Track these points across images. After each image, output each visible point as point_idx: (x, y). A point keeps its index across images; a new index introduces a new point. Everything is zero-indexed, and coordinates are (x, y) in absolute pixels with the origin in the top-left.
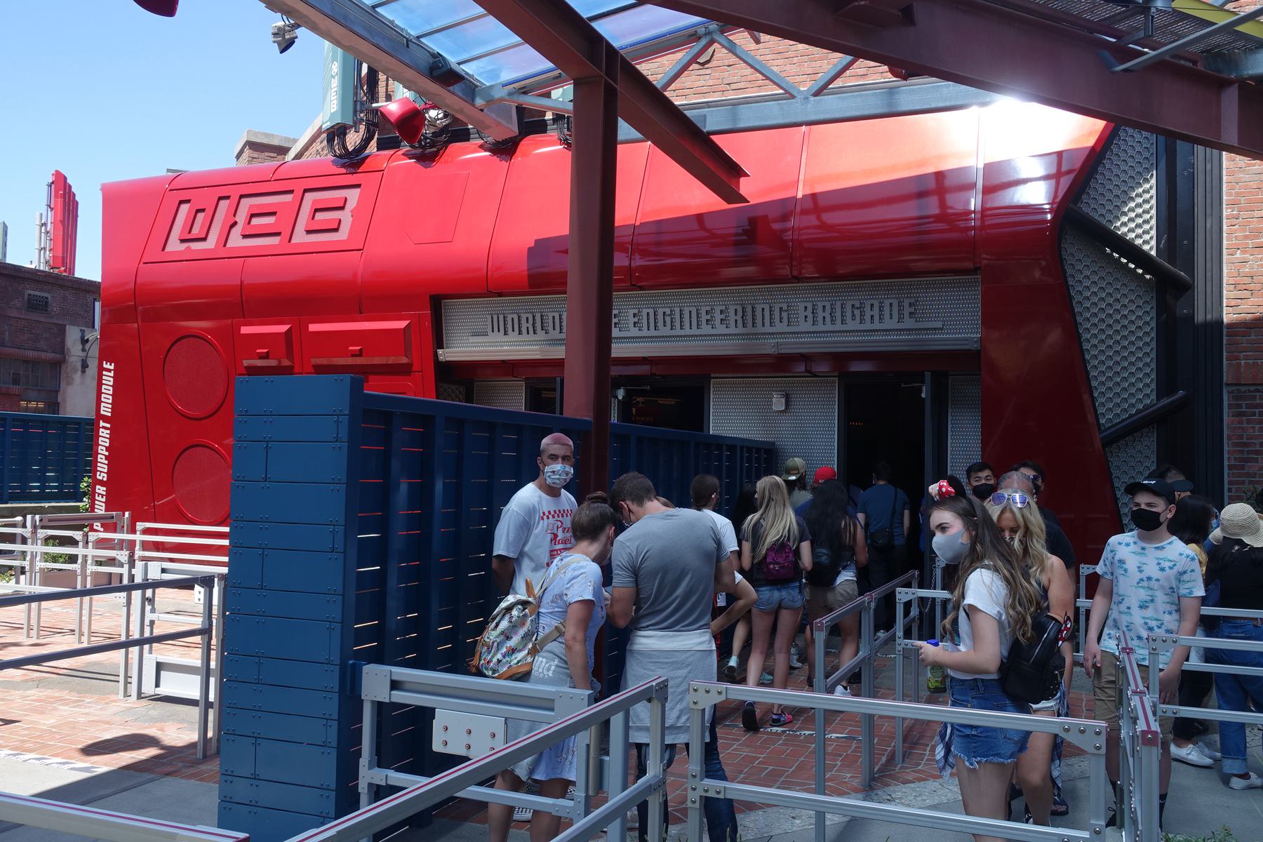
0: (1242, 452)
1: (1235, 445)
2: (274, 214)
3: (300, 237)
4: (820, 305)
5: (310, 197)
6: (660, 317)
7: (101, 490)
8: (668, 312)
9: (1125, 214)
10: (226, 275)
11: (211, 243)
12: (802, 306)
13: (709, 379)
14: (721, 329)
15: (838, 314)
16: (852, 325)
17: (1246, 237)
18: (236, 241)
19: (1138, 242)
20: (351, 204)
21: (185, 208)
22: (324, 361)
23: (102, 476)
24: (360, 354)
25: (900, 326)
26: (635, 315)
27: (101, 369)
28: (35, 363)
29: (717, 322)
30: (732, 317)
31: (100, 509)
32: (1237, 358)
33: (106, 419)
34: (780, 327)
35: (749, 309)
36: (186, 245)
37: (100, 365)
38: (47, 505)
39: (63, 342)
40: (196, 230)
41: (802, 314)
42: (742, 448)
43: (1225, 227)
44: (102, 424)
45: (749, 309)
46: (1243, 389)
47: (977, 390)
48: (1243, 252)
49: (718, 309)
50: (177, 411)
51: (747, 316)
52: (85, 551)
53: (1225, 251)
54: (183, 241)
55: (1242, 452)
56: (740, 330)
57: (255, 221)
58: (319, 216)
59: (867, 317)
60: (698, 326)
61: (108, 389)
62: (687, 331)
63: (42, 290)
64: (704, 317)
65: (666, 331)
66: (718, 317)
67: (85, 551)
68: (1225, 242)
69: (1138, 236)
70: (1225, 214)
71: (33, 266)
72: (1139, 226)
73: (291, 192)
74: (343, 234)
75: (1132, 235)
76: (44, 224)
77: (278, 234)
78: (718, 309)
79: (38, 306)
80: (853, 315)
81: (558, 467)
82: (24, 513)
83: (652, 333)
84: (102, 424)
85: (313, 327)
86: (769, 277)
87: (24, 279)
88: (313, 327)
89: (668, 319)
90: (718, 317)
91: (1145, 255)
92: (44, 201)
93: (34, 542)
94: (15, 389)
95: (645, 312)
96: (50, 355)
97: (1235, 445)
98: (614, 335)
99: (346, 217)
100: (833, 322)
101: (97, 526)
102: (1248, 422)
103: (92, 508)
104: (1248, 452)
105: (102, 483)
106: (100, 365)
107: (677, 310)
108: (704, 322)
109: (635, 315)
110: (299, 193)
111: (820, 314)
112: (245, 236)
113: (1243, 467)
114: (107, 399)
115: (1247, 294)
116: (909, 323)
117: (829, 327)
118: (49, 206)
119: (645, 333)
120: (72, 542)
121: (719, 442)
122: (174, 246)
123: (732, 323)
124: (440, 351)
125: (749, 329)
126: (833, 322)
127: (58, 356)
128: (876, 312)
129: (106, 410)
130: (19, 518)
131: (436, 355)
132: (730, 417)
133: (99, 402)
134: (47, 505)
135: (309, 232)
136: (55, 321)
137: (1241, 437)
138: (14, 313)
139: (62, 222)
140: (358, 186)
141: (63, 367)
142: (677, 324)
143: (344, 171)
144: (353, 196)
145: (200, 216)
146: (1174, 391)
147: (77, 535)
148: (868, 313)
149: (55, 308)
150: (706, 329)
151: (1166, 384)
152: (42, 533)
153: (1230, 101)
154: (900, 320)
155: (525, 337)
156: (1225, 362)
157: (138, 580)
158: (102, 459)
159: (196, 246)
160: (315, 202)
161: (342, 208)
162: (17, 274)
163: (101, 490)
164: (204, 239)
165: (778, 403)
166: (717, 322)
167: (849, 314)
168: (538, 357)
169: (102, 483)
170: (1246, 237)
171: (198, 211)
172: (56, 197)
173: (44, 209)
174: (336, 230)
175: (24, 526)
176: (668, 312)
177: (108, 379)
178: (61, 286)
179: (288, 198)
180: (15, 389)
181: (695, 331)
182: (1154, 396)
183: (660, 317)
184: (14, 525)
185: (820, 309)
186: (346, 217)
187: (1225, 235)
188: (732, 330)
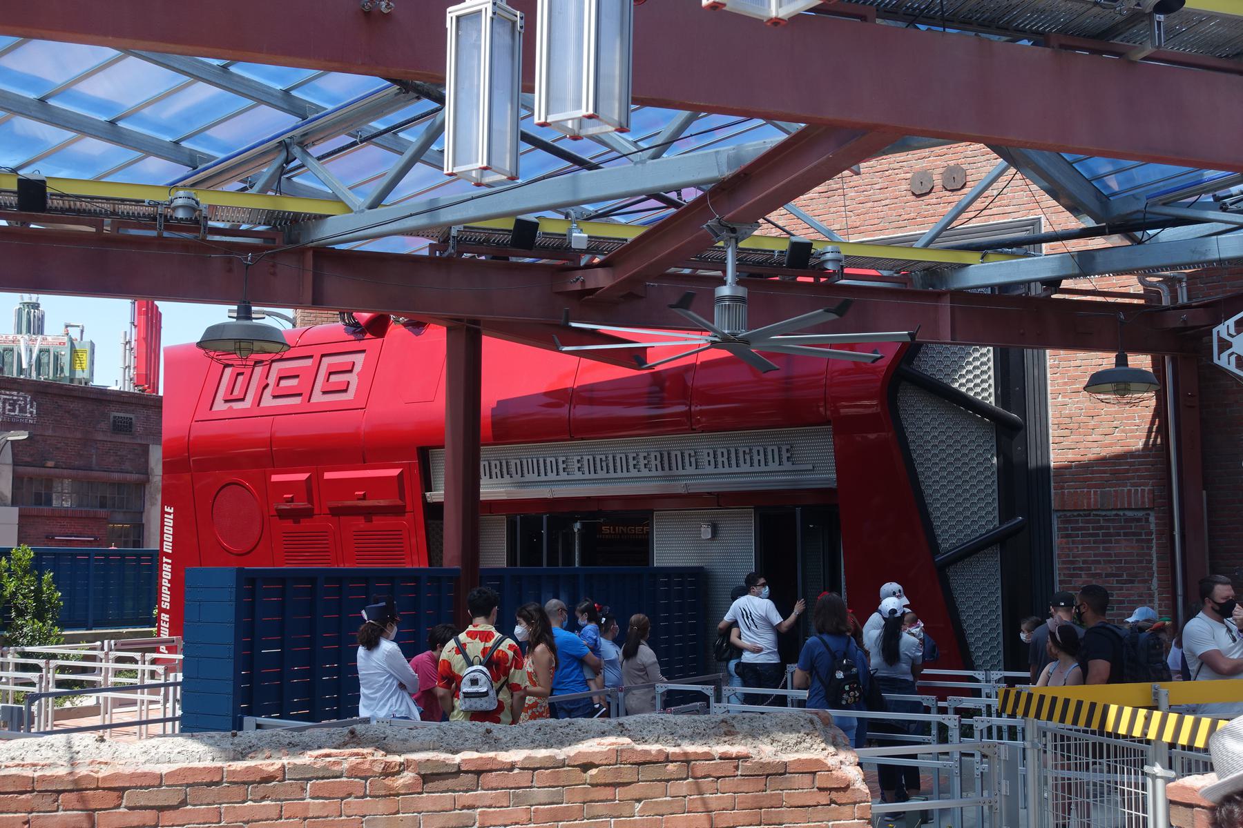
0: (1068, 569)
1: (1064, 562)
2: (297, 376)
3: (318, 397)
5: (326, 361)
7: (165, 617)
9: (969, 363)
10: (262, 429)
11: (247, 404)
12: (706, 452)
14: (645, 472)
16: (745, 468)
17: (1065, 384)
18: (268, 401)
19: (963, 390)
20: (357, 369)
21: (228, 371)
22: (339, 504)
23: (166, 606)
24: (364, 498)
25: (781, 468)
27: (163, 513)
28: (120, 485)
30: (653, 462)
31: (165, 635)
32: (1062, 488)
33: (168, 555)
34: (690, 470)
35: (666, 455)
36: (228, 405)
37: (163, 509)
38: (125, 631)
39: (147, 462)
40: (236, 392)
43: (1049, 375)
44: (165, 560)
45: (666, 455)
46: (1068, 514)
47: (863, 515)
48: (1064, 397)
50: (224, 548)
51: (665, 461)
52: (143, 667)
53: (1049, 396)
54: (226, 401)
55: (1068, 569)
56: (660, 473)
57: (284, 383)
58: (333, 378)
61: (169, 530)
62: (619, 474)
63: (126, 412)
67: (143, 667)
68: (1049, 388)
69: (971, 389)
70: (1049, 363)
71: (117, 388)
72: (976, 377)
73: (311, 357)
74: (350, 396)
76: (129, 342)
77: (300, 395)
78: (641, 455)
79: (123, 427)
82: (101, 637)
83: (593, 476)
84: (165, 560)
85: (328, 475)
86: (685, 424)
87: (110, 401)
88: (328, 475)
89: (604, 464)
90: (642, 462)
92: (128, 319)
93: (107, 661)
94: (102, 512)
95: (586, 458)
96: (134, 477)
97: (1064, 562)
99: (353, 379)
101: (163, 648)
102: (1074, 542)
103: (159, 634)
104: (1074, 569)
105: (165, 611)
106: (163, 509)
110: (317, 357)
111: (720, 459)
112: (275, 397)
113: (1070, 582)
114: (168, 538)
115: (1067, 432)
116: (787, 466)
117: (727, 470)
118: (133, 323)
119: (587, 476)
120: (132, 660)
122: (220, 406)
124: (428, 494)
125: (667, 472)
127: (142, 477)
128: (762, 457)
129: (168, 548)
130: (98, 643)
131: (424, 496)
133: (162, 541)
134: (125, 631)
135: (324, 393)
136: (139, 441)
137: (1068, 555)
138: (100, 437)
139: (145, 339)
140: (364, 351)
141: (147, 486)
143: (352, 337)
144: (359, 359)
145: (240, 378)
146: (1014, 516)
147: (137, 655)
149: (138, 428)
150: (634, 473)
151: (1006, 511)
152: (113, 654)
153: (946, 304)
155: (494, 480)
156: (1053, 491)
157: (171, 688)
158: (165, 590)
159: (237, 406)
160: (330, 365)
161: (351, 371)
162: (103, 397)
163: (165, 617)
164: (243, 400)
165: (706, 533)
169: (165, 611)
170: (1065, 384)
171: (238, 374)
172: (139, 314)
173: (127, 326)
174: (345, 391)
175: (102, 649)
177: (169, 521)
178: (144, 406)
179: (308, 362)
180: (102, 512)
181: (625, 474)
182: (997, 523)
184: (94, 649)
186: (353, 379)
187: (1049, 382)
188: (654, 473)
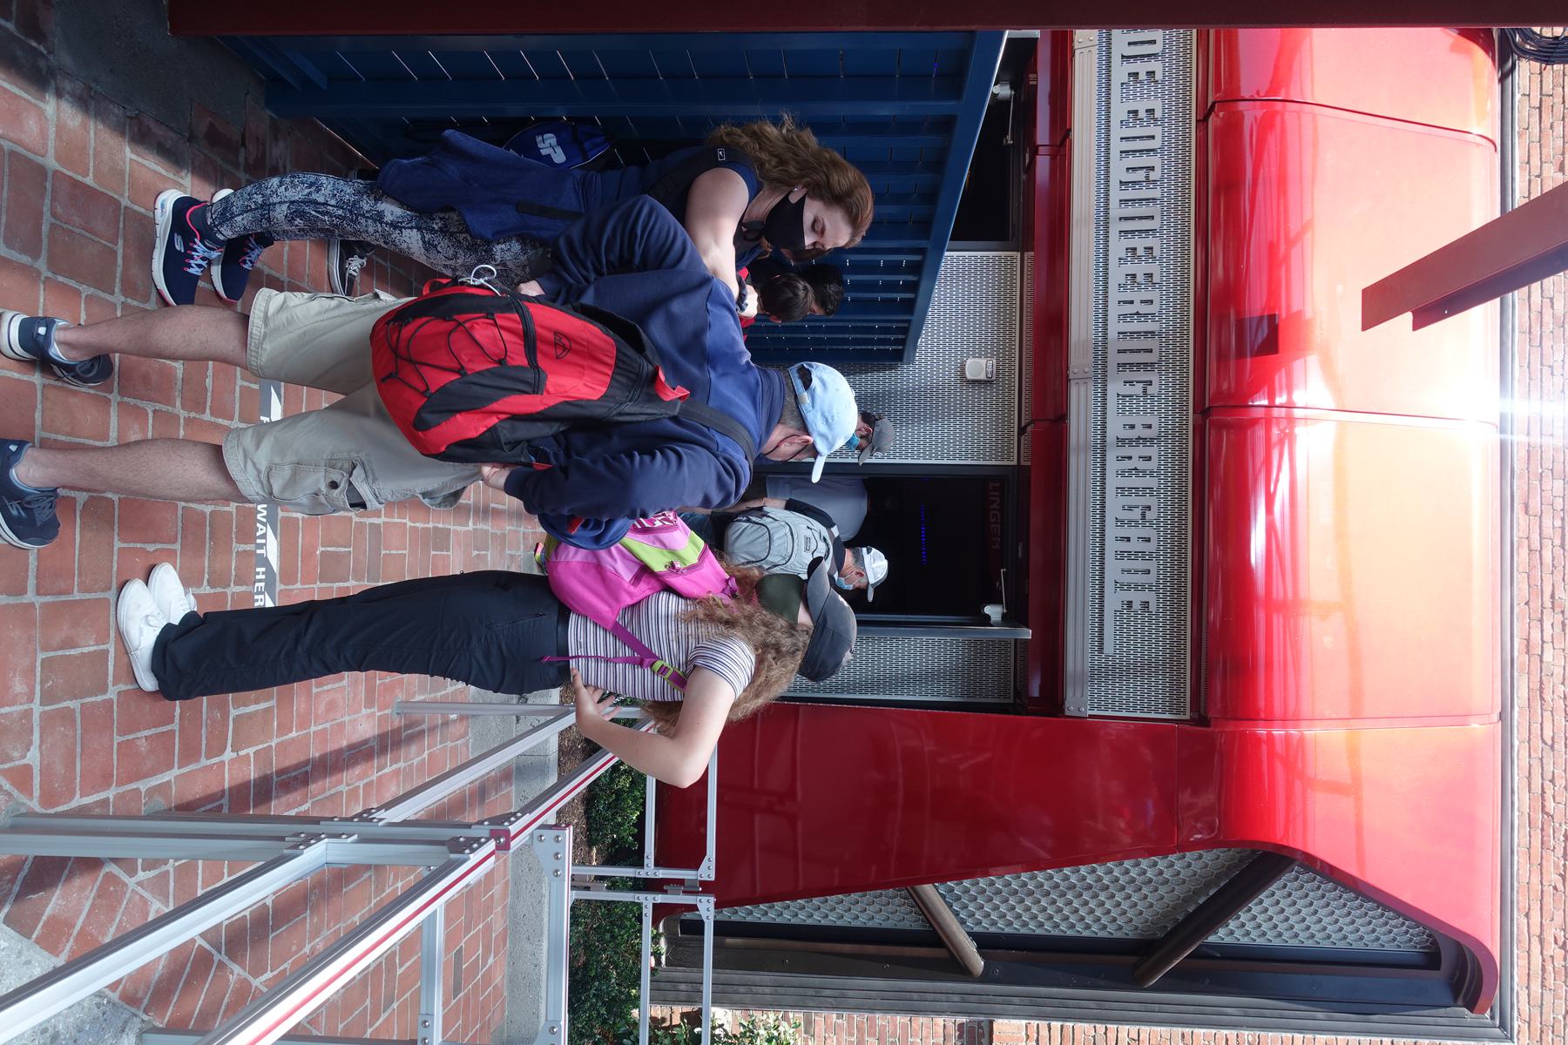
4: (1152, 451)
6: (1145, 161)
8: (1153, 176)
13: (1023, 249)
15: (1135, 482)
16: (1115, 506)
26: (1150, 111)
29: (1130, 268)
41: (1138, 420)
42: (909, 321)
49: (1154, 268)
56: (1114, 343)
59: (1125, 532)
60: (1121, 490)
64: (1140, 243)
65: (1118, 171)
66: (1140, 269)
75: (1256, 910)
78: (1154, 268)
80: (1130, 508)
81: (847, 420)
83: (1116, 146)
89: (1140, 175)
90: (1140, 269)
91: (1211, 927)
95: (1157, 131)
98: (1116, 33)
100: (1121, 555)
107: (1156, 193)
108: (1131, 243)
109: (1150, 111)
121: (920, 272)
123: (1128, 296)
126: (1123, 317)
128: (1135, 546)
132: (965, 298)
142: (1130, 194)
148: (1133, 533)
154: (1120, 586)
165: (978, 367)
166: (1130, 268)
167: (1133, 500)
168: (1070, 665)
176: (1153, 176)
183: (1145, 161)
185: (1146, 451)
188: (1114, 327)
